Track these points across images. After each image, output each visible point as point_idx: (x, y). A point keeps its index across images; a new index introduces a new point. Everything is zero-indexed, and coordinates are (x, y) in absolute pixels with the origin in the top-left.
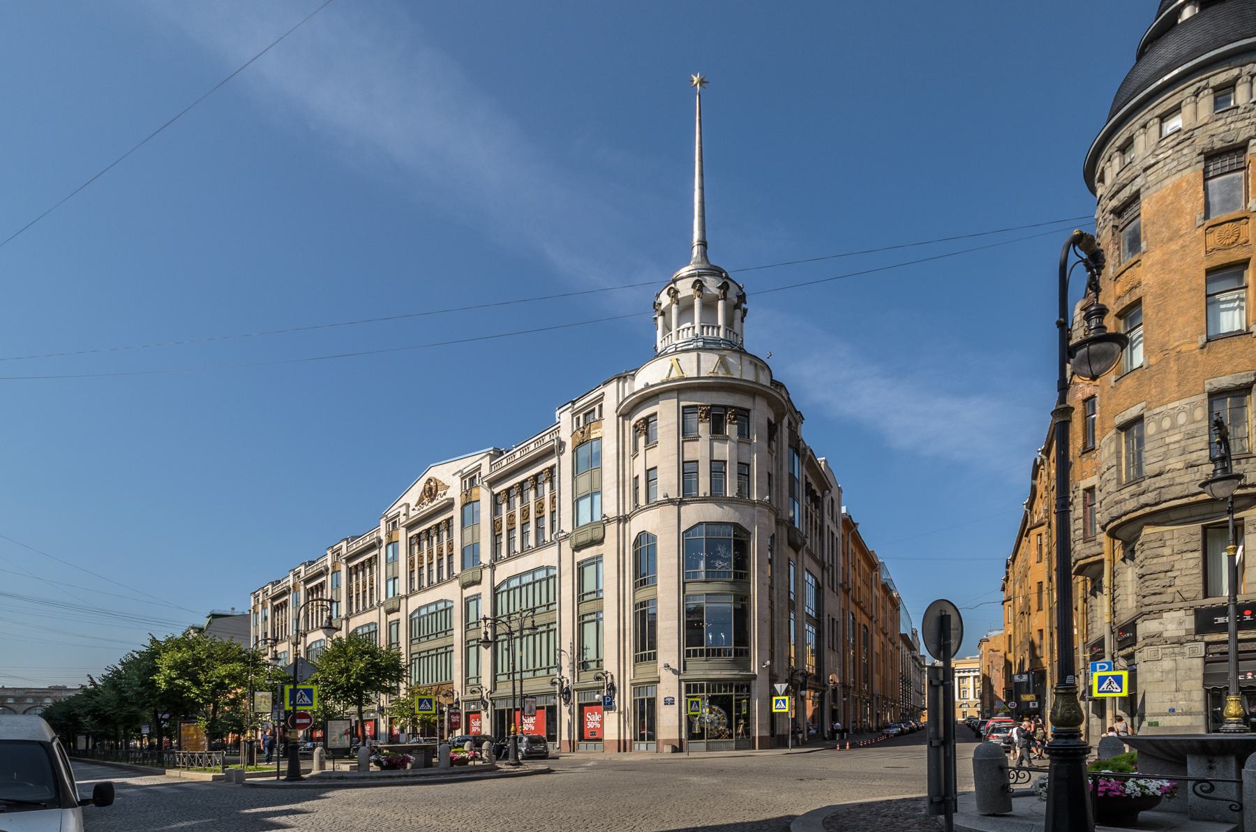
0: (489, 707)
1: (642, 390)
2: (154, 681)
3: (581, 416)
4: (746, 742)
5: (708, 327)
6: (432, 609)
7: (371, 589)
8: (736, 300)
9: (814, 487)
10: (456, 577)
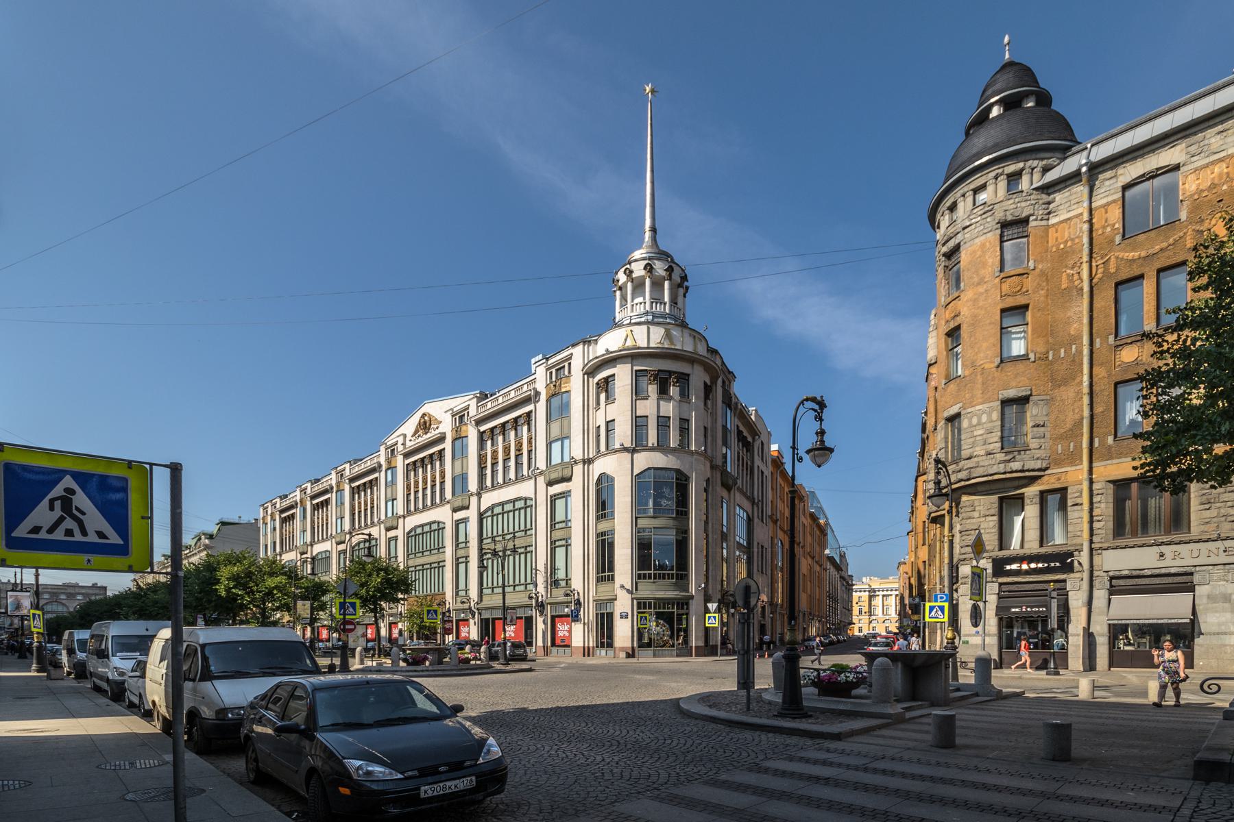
0: (476, 616)
1: (603, 355)
2: (217, 589)
3: (554, 370)
4: (685, 651)
5: (657, 303)
6: (427, 529)
7: (372, 508)
9: (745, 433)
10: (448, 502)
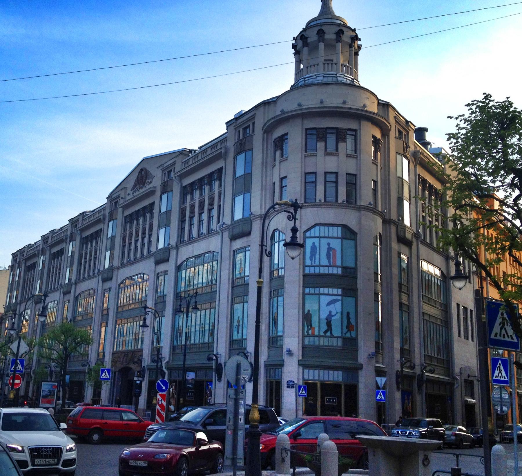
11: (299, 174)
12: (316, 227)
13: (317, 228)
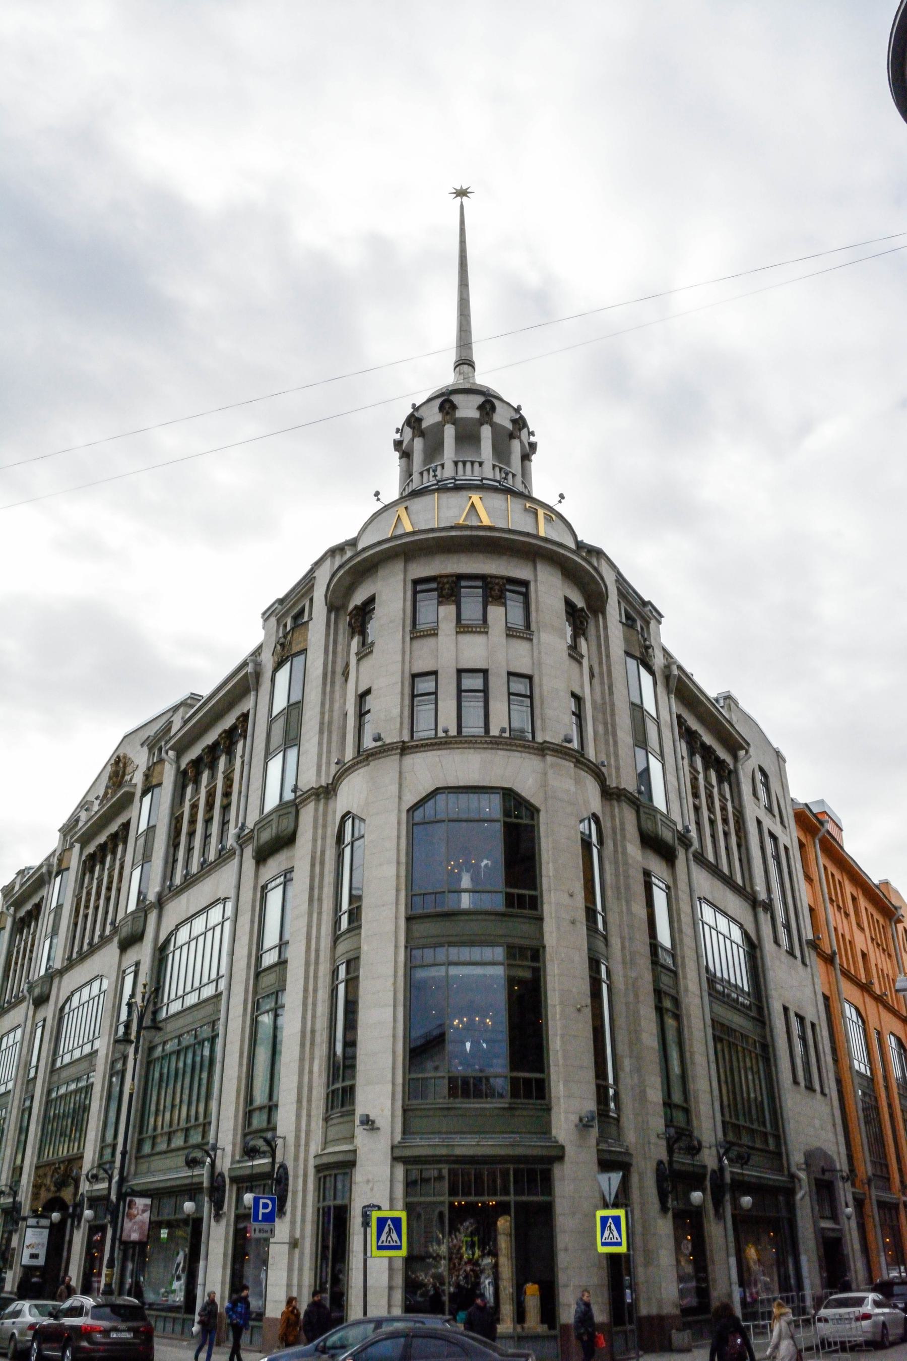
5: (464, 463)
8: (510, 426)
11: (397, 678)
12: (438, 797)
13: (441, 798)
